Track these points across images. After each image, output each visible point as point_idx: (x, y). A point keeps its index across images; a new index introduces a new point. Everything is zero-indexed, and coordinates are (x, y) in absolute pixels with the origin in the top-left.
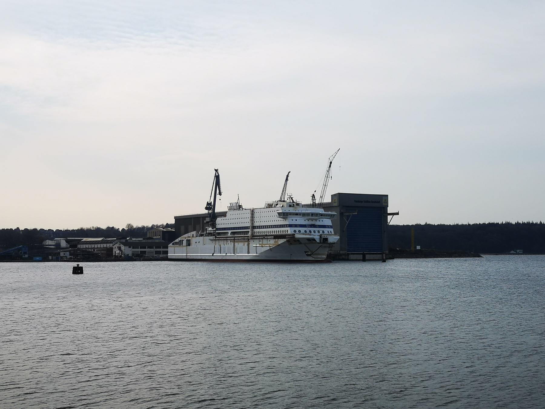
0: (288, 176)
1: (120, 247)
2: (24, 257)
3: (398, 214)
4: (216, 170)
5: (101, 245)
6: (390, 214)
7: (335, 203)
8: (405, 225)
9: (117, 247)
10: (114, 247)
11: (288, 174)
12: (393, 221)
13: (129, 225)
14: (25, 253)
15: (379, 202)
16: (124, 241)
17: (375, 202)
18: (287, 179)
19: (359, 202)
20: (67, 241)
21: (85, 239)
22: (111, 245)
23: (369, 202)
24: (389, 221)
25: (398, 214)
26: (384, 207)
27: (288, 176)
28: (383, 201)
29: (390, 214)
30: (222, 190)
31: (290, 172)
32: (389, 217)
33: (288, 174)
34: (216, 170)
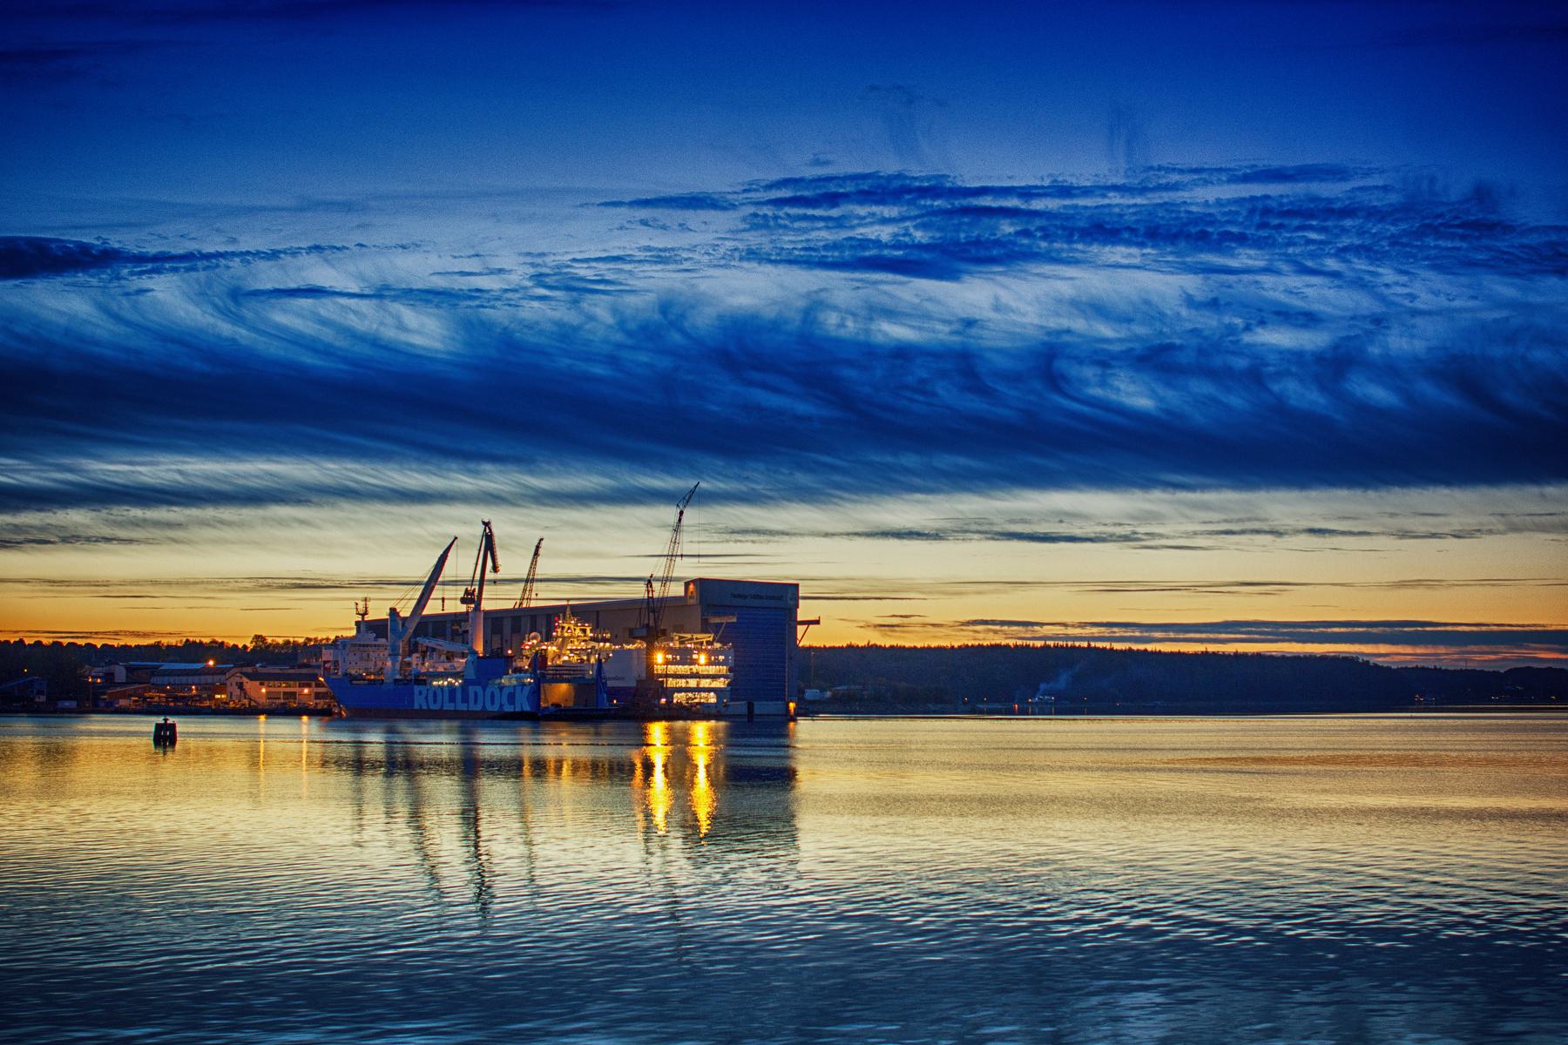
0: (538, 547)
1: (242, 683)
2: (37, 700)
3: (817, 622)
4: (486, 524)
5: (202, 677)
6: (803, 623)
7: (691, 597)
8: (827, 646)
9: (234, 684)
10: (228, 683)
11: (539, 543)
12: (807, 638)
13: (257, 637)
14: (40, 693)
15: (780, 598)
16: (249, 670)
17: (772, 598)
18: (536, 554)
19: (740, 596)
20: (694, 662)
21: (166, 666)
22: (223, 677)
23: (761, 598)
24: (799, 637)
25: (817, 622)
26: (790, 609)
27: (538, 547)
28: (790, 595)
29: (803, 623)
30: (500, 561)
31: (542, 540)
32: (801, 629)
33: (539, 543)
34: (486, 524)
